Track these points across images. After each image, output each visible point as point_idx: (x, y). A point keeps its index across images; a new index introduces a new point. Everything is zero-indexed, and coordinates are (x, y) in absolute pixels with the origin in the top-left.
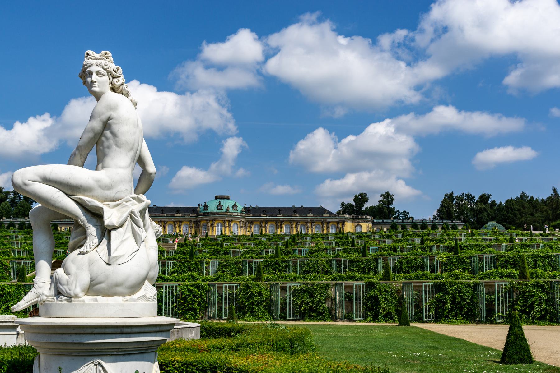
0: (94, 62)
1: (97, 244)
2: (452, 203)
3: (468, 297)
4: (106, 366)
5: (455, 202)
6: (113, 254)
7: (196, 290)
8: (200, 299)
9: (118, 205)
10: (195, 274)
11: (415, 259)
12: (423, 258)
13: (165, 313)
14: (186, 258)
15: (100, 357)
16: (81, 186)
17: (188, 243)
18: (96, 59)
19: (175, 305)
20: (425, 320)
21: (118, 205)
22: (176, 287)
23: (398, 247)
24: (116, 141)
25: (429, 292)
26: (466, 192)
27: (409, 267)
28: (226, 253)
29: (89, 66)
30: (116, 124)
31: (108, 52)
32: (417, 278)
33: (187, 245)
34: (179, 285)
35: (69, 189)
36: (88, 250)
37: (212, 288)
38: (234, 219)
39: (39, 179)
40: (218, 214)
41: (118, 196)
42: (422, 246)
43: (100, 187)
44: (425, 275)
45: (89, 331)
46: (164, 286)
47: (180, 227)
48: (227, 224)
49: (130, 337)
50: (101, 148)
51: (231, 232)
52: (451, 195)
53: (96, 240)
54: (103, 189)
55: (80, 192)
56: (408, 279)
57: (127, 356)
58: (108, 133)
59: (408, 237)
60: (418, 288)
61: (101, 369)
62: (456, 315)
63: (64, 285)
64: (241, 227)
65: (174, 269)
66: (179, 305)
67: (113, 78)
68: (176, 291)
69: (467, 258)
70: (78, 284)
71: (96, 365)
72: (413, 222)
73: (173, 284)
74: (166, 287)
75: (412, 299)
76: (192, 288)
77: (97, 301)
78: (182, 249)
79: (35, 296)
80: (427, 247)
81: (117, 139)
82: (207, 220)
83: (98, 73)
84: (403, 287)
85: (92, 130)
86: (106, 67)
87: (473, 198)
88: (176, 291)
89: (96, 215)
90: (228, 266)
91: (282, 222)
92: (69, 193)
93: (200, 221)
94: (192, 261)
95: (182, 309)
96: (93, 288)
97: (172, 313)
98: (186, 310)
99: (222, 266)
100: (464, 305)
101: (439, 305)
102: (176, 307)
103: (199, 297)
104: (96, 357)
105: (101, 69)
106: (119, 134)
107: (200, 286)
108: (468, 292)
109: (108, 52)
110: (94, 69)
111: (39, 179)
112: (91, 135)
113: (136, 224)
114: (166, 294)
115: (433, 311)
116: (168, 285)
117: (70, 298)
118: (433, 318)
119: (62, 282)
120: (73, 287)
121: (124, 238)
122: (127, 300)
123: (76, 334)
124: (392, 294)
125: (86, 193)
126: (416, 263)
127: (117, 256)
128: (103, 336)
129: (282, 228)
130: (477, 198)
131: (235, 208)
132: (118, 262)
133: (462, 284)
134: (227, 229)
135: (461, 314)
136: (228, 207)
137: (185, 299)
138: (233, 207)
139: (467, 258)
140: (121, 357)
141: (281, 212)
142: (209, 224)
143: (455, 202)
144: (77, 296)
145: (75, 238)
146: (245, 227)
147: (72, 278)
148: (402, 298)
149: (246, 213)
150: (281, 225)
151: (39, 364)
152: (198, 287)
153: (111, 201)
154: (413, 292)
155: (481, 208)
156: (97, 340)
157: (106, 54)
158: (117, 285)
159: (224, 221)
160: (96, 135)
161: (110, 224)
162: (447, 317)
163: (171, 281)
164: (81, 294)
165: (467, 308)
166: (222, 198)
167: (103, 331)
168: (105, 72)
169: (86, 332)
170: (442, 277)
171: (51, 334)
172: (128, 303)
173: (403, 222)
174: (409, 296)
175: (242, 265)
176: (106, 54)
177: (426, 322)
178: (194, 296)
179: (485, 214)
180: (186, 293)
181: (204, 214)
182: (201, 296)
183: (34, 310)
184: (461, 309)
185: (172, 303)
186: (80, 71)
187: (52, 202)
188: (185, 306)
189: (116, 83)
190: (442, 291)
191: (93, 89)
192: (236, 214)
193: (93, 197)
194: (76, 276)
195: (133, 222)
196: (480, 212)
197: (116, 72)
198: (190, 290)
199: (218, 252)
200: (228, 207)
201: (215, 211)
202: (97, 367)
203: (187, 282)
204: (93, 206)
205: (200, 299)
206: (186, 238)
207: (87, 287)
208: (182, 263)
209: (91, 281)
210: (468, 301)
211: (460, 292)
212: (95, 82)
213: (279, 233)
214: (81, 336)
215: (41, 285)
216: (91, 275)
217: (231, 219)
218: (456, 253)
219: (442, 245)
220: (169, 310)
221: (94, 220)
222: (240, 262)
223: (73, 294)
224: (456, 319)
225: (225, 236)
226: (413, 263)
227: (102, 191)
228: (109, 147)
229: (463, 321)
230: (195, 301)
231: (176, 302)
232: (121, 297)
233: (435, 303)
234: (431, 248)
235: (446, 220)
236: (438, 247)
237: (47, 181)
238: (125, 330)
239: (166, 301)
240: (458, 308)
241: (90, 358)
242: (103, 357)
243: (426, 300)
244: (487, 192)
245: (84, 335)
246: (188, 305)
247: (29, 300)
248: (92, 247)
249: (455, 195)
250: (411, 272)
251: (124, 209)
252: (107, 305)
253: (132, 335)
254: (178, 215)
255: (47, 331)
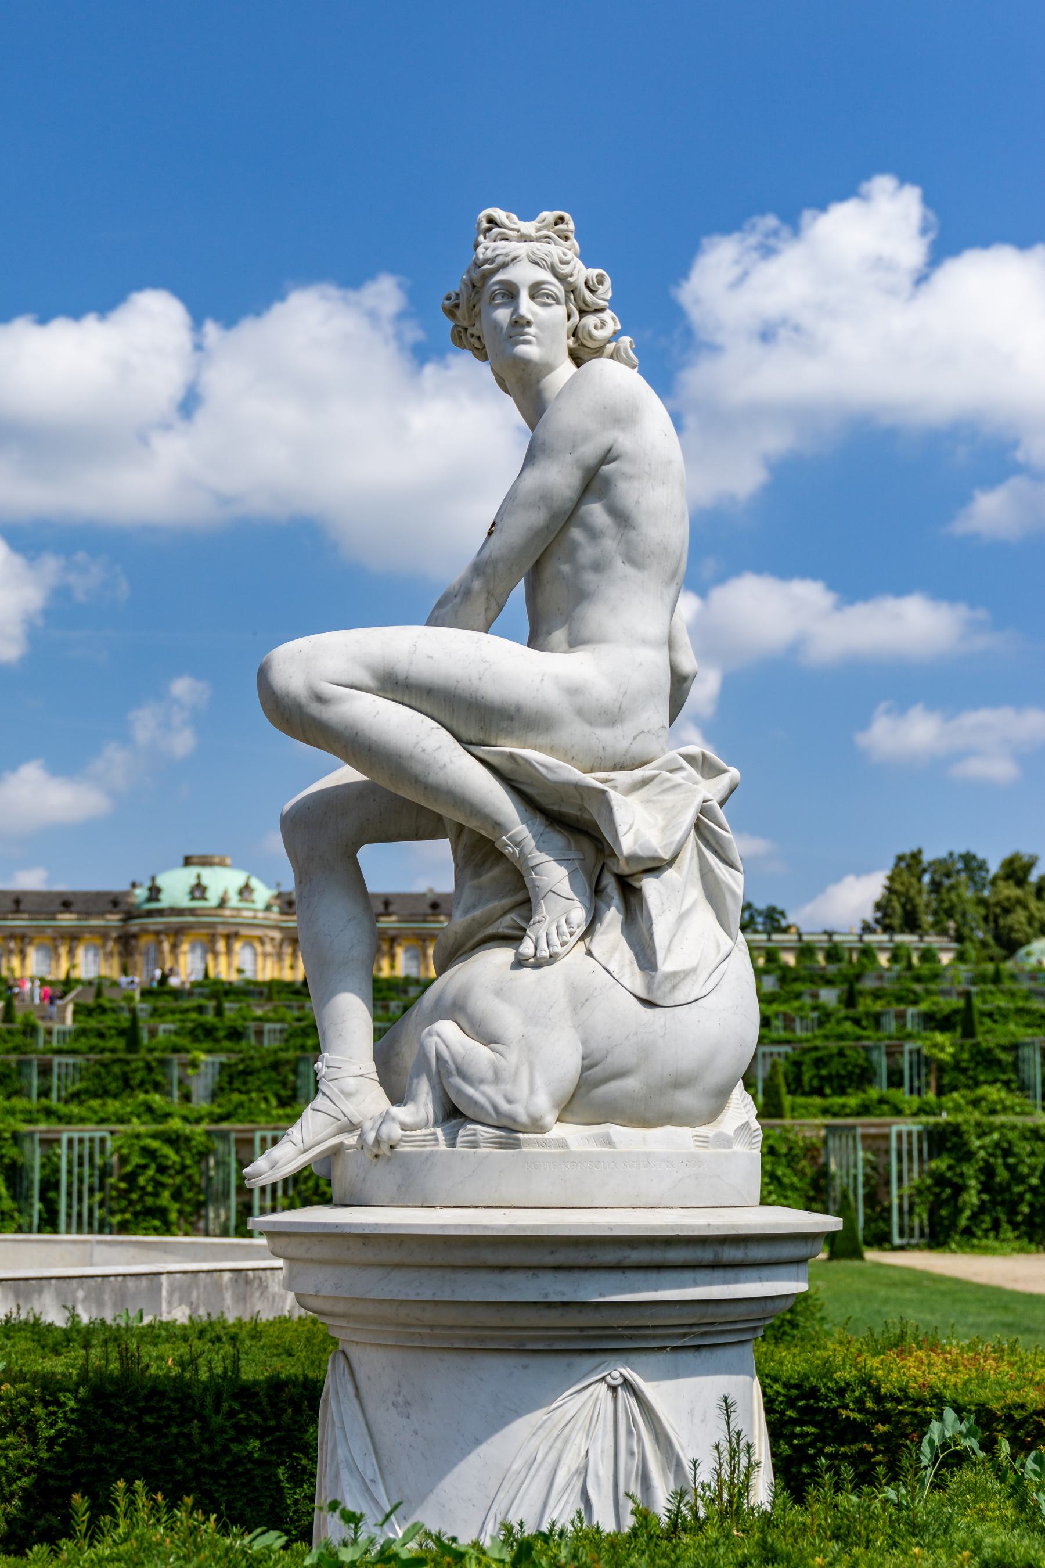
0: (514, 248)
1: (584, 928)
2: (919, 880)
3: (1033, 1168)
4: (660, 1393)
5: (926, 878)
6: (666, 965)
7: (167, 1150)
8: (178, 1180)
9: (645, 782)
10: (157, 1099)
11: (841, 1053)
12: (867, 1049)
13: (69, 1225)
14: (113, 1051)
15: (623, 1357)
16: (518, 709)
17: (108, 1005)
18: (525, 238)
19: (98, 1196)
20: (897, 1241)
21: (645, 782)
22: (103, 1140)
23: (777, 1015)
24: (629, 543)
25: (910, 1153)
26: (960, 849)
27: (821, 1078)
28: (236, 1034)
29: (504, 266)
30: (629, 477)
31: (566, 215)
32: (865, 1110)
33: (103, 1010)
34: (112, 1133)
35: (471, 716)
36: (558, 949)
37: (219, 1145)
38: (244, 931)
39: (368, 680)
40: (192, 912)
41: (639, 748)
42: (851, 1013)
43: (580, 712)
44: (887, 1102)
45: (609, 1256)
46: (64, 1137)
47: (71, 953)
48: (221, 946)
49: (737, 1281)
50: (566, 568)
51: (240, 971)
52: (916, 856)
53: (579, 914)
54: (591, 724)
55: (509, 733)
56: (835, 1115)
57: (705, 1353)
58: (596, 512)
59: (798, 987)
60: (877, 1143)
61: (633, 1402)
62: (996, 1226)
63: (482, 1081)
64: (265, 955)
65: (78, 1086)
66: (112, 1198)
67: (582, 313)
68: (103, 1151)
69: (1004, 1048)
70: (539, 1081)
71: (613, 1389)
72: (800, 940)
73: (91, 1131)
74: (70, 1141)
75: (855, 1177)
76: (155, 1144)
77: (609, 1142)
78: (92, 1023)
79: (331, 1130)
80: (868, 1015)
81: (632, 535)
82: (158, 933)
83: (536, 291)
84: (825, 1141)
85: (544, 497)
86: (565, 270)
87: (982, 866)
88: (103, 1151)
89: (576, 823)
90: (251, 1073)
91: (393, 941)
92: (472, 734)
93: (135, 936)
94: (137, 1061)
95: (123, 1211)
96: (590, 1095)
97: (90, 1224)
98: (136, 1214)
99: (231, 1077)
100: (1021, 1196)
101: (944, 1192)
102: (102, 1204)
103: (178, 1173)
104: (611, 1358)
105: (546, 276)
106: (641, 518)
107: (178, 1137)
108: (1032, 1154)
109: (566, 215)
110: (523, 274)
111: (368, 680)
112: (536, 518)
113: (716, 853)
114: (70, 1163)
115: (922, 1214)
116: (76, 1136)
117: (509, 1131)
118: (922, 1235)
119: (471, 1071)
120: (522, 1091)
121: (684, 908)
122: (704, 1141)
123: (557, 1268)
124: (791, 1159)
125: (531, 737)
126: (845, 1065)
127: (675, 974)
128: (653, 1276)
129: (393, 957)
130: (994, 867)
131: (246, 894)
132: (680, 996)
133: (1014, 1128)
134: (223, 960)
135: (1010, 1222)
136: (225, 893)
137: (131, 1178)
138: (241, 892)
139: (1004, 1048)
140: (688, 1357)
141: (392, 908)
142: (166, 946)
143: (926, 878)
144: (537, 1126)
145: (474, 907)
146: (280, 956)
147: (512, 1058)
148: (823, 1172)
149: (282, 913)
150: (392, 947)
151: (357, 1388)
152: (174, 1140)
153: (615, 768)
154: (861, 1154)
155: (1008, 899)
156: (632, 1291)
157: (561, 220)
158: (679, 1083)
159: (213, 938)
160: (554, 517)
161: (640, 853)
162: (968, 1232)
163: (82, 1120)
164: (550, 1118)
165: (1031, 1205)
166: (206, 862)
167: (656, 1255)
168: (558, 289)
169: (595, 1262)
170: (941, 1108)
171: (454, 1268)
172: (712, 1151)
173: (769, 940)
174: (847, 1167)
175: (295, 1072)
176: (561, 220)
177: (902, 1248)
178: (162, 1169)
179: (1019, 916)
180: (136, 1160)
181: (150, 913)
182: (184, 1167)
183: (309, 1187)
184: (1012, 1209)
185: (91, 1190)
186: (455, 283)
187: (418, 768)
188: (131, 1203)
189: (595, 332)
190: (950, 1150)
191: (522, 349)
192: (250, 914)
193: (552, 750)
194: (529, 1048)
195: (708, 844)
196: (1007, 911)
197: (592, 291)
198: (146, 1151)
199: (209, 1032)
200: (225, 893)
201: (185, 902)
202: (615, 1399)
203: (136, 1125)
204: (556, 783)
205: (178, 1180)
206: (98, 986)
207: (570, 1087)
208: (105, 1065)
209: (585, 1069)
210: (1034, 1181)
211: (1007, 1153)
212: (529, 323)
213: (385, 973)
214: (576, 1275)
215: (351, 1084)
216: (584, 1042)
217: (233, 929)
218: (969, 1032)
219: (911, 1010)
220: (80, 1215)
221: (558, 839)
222: (288, 1062)
223: (523, 1118)
224: (997, 1237)
225: (217, 982)
226: (835, 1066)
227: (587, 729)
228: (598, 567)
229: (1016, 1244)
230: (164, 1186)
231: (102, 1188)
232: (686, 1132)
233: (928, 1188)
234: (877, 1019)
235: (902, 932)
236: (901, 1016)
237: (395, 686)
238: (730, 1254)
239: (70, 1185)
240: (1002, 1203)
241: (589, 1361)
242: (634, 1358)
243: (900, 1179)
244: (1026, 850)
245: (586, 1275)
246: (141, 1199)
247: (309, 1140)
248: (567, 938)
249: (927, 857)
250: (828, 1091)
251: (670, 798)
252: (648, 1158)
253: (744, 1273)
254: (67, 916)
255: (439, 1258)
